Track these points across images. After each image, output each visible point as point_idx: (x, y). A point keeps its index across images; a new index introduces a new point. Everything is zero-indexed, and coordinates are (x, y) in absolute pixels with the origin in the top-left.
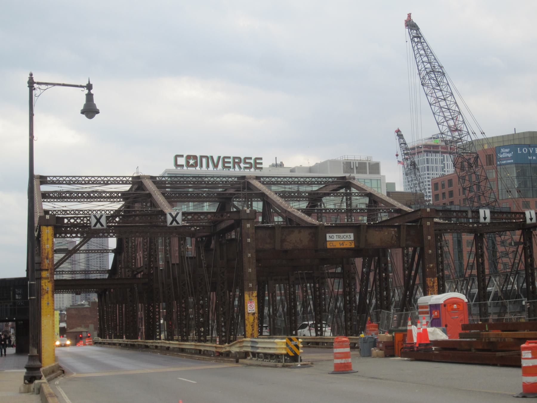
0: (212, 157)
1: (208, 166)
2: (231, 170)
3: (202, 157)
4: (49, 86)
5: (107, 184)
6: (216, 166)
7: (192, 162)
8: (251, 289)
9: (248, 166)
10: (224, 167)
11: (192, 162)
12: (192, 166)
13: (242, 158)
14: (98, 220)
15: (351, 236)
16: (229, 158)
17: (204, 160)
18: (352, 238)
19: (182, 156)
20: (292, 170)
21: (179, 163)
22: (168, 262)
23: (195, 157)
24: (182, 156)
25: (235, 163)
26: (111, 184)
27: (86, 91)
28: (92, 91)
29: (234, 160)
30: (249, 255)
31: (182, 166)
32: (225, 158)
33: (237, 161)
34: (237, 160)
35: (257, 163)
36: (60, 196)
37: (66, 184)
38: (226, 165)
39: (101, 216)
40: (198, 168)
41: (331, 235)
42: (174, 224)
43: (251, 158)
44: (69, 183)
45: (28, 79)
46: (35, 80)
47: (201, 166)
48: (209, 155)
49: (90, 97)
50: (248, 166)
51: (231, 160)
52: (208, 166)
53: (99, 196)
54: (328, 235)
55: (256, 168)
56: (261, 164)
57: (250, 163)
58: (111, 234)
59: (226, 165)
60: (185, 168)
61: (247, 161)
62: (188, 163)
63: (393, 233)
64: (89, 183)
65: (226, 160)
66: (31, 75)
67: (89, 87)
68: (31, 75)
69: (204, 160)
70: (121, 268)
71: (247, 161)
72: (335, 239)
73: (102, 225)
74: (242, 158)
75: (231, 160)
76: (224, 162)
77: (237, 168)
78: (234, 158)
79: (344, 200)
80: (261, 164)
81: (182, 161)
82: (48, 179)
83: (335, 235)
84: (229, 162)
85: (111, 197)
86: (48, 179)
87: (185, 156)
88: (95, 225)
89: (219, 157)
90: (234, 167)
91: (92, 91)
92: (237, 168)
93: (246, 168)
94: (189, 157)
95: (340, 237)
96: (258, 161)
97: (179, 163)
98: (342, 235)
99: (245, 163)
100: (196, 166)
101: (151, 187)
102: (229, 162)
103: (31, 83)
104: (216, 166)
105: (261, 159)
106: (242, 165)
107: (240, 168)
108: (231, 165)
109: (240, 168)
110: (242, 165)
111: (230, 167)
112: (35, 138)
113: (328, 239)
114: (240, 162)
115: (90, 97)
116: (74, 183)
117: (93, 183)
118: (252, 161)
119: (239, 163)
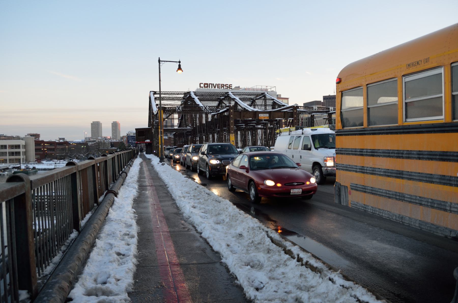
0: (213, 84)
1: (212, 87)
2: (221, 89)
3: (210, 84)
4: (165, 62)
5: (178, 94)
6: (215, 87)
7: (206, 86)
8: (232, 133)
9: (227, 87)
10: (218, 88)
11: (206, 86)
12: (206, 87)
13: (225, 84)
14: (206, 108)
15: (268, 115)
16: (220, 84)
17: (211, 85)
18: (268, 116)
19: (202, 83)
20: (245, 89)
21: (201, 86)
22: (201, 123)
23: (207, 84)
24: (202, 83)
25: (222, 86)
26: (180, 94)
27: (178, 64)
28: (180, 64)
29: (222, 85)
30: (232, 121)
31: (202, 87)
32: (218, 84)
33: (223, 86)
34: (223, 85)
35: (230, 87)
36: (169, 99)
37: (164, 94)
38: (219, 87)
39: (207, 106)
40: (208, 88)
41: (261, 114)
42: (179, 110)
43: (228, 85)
44: (168, 94)
45: (158, 60)
46: (161, 60)
47: (209, 87)
48: (212, 83)
49: (180, 66)
50: (227, 87)
51: (220, 85)
52: (212, 87)
53: (173, 99)
54: (259, 115)
55: (230, 88)
56: (232, 87)
57: (228, 86)
58: (176, 113)
59: (219, 87)
60: (203, 88)
61: (227, 86)
62: (204, 86)
63: (283, 114)
64: (171, 94)
65: (219, 85)
66: (159, 58)
67: (180, 62)
68: (159, 58)
69: (211, 85)
70: (184, 125)
71: (227, 86)
72: (262, 116)
73: (180, 110)
74: (225, 84)
75: (220, 85)
76: (218, 86)
77: (223, 88)
78: (222, 85)
79: (264, 101)
80: (232, 87)
81: (202, 85)
82: (157, 92)
83: (262, 114)
84: (220, 86)
85: (178, 99)
86: (157, 92)
87: (203, 83)
88: (178, 110)
89: (216, 84)
90: (222, 88)
91: (180, 64)
92: (223, 88)
93: (226, 88)
94: (205, 84)
95: (264, 115)
96: (230, 86)
97: (201, 86)
98: (264, 114)
99: (226, 86)
100: (208, 87)
101: (193, 96)
102: (220, 86)
103: (159, 61)
104: (215, 87)
105: (232, 85)
106: (225, 87)
107: (224, 88)
108: (220, 87)
109: (224, 88)
110: (225, 87)
111: (220, 88)
112: (161, 81)
113: (260, 116)
114: (224, 86)
115: (180, 66)
116: (166, 94)
117: (173, 94)
118: (228, 86)
119: (223, 87)
